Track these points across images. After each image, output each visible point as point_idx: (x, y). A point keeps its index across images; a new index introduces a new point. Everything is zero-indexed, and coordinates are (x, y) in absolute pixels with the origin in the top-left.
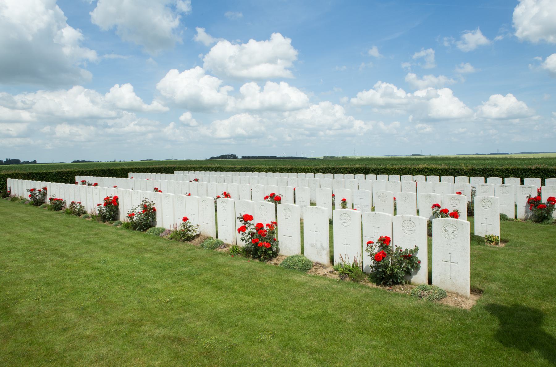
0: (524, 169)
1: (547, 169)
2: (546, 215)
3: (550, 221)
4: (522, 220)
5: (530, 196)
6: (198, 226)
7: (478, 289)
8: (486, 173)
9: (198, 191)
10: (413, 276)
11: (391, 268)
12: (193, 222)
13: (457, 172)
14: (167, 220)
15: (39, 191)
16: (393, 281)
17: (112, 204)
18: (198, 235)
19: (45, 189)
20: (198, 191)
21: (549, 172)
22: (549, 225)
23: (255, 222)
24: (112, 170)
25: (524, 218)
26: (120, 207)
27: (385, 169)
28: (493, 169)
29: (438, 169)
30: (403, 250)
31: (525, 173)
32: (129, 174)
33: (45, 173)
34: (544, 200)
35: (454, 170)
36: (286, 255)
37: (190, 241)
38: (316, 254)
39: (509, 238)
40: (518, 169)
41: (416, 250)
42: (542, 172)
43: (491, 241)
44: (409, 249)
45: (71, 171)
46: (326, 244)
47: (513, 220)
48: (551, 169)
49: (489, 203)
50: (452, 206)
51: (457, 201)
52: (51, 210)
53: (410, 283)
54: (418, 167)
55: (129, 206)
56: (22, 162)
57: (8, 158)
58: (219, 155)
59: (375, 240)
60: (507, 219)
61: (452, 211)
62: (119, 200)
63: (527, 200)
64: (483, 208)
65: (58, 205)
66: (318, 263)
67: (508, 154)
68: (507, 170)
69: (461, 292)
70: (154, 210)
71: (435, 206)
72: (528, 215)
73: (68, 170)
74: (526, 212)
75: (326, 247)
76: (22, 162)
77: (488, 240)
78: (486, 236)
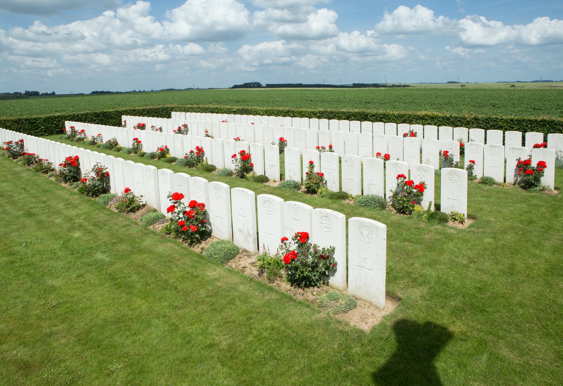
0: (529, 120)
1: (554, 121)
2: (533, 182)
3: (538, 188)
4: (510, 184)
5: (520, 159)
6: (142, 196)
7: (398, 297)
8: (489, 123)
9: (174, 144)
10: (331, 277)
11: (307, 268)
12: (136, 192)
13: (459, 121)
14: (117, 188)
15: (17, 143)
16: (306, 284)
17: (73, 163)
18: (144, 206)
19: (22, 141)
20: (174, 144)
21: (556, 124)
22: (534, 194)
23: (186, 202)
24: (106, 112)
25: (513, 182)
26: (81, 167)
27: (384, 114)
28: (497, 119)
29: (440, 117)
30: (320, 249)
31: (531, 124)
32: (122, 116)
33: (35, 119)
34: (534, 164)
35: (456, 118)
36: (219, 237)
37: (134, 212)
38: (243, 241)
39: (478, 215)
40: (524, 120)
41: (333, 250)
42: (548, 124)
43: (455, 219)
44: (326, 248)
45: (62, 116)
46: (253, 232)
47: (500, 185)
48: (558, 121)
49: (456, 177)
50: (418, 177)
51: (424, 172)
52: (332, 23)
53: (328, 284)
54: (419, 113)
55: (87, 168)
56: (40, 94)
57: (27, 90)
58: (242, 83)
59: (290, 235)
60: (494, 183)
61: (418, 184)
62: (80, 160)
63: (516, 163)
64: (450, 182)
65: (30, 160)
66: (245, 251)
67: (552, 81)
68: (512, 120)
69: (375, 301)
70: (108, 174)
71: (399, 176)
72: (517, 179)
73: (58, 114)
74: (515, 176)
75: (252, 234)
76: (40, 94)
77: (453, 218)
78: (452, 213)
